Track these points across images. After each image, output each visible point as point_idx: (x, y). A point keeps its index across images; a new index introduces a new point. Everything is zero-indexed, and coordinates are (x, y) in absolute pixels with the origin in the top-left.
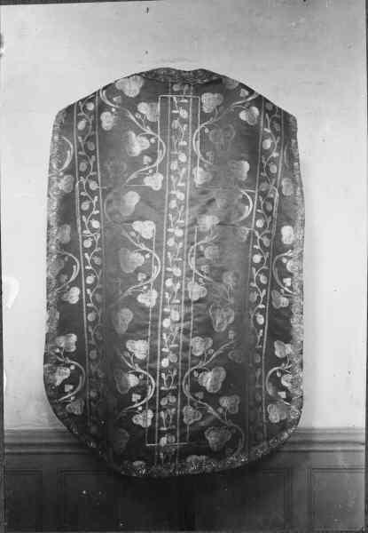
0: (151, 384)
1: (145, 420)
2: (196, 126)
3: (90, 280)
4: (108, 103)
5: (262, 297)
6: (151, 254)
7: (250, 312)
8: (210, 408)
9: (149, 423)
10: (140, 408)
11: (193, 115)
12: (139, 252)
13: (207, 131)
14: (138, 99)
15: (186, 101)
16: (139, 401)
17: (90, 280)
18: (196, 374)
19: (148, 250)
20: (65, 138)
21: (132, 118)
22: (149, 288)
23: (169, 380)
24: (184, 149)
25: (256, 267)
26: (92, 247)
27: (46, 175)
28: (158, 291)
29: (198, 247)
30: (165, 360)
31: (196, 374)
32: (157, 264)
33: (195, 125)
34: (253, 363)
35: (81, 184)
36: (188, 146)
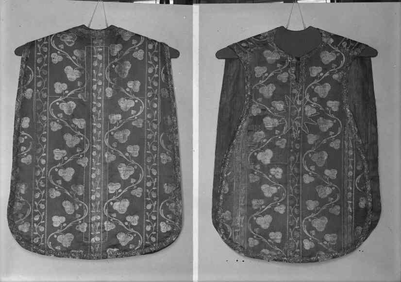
0: (86, 208)
1: (83, 229)
2: (107, 64)
3: (39, 84)
4: (53, 182)
5: (154, 158)
6: (84, 138)
7: (36, 181)
8: (121, 222)
9: (85, 230)
10: (80, 222)
11: (105, 58)
12: (77, 136)
13: (114, 66)
14: (74, 48)
15: (101, 49)
16: (80, 218)
17: (39, 84)
18: (111, 203)
19: (82, 135)
20: (29, 67)
21: (70, 58)
22: (83, 156)
23: (96, 207)
24: (100, 78)
25: (149, 141)
26: (42, 64)
27: (16, 88)
28: (89, 158)
29: (110, 133)
30: (93, 196)
31: (111, 203)
32: (87, 143)
33: (106, 63)
34: (151, 198)
35: (37, 94)
36: (103, 76)
